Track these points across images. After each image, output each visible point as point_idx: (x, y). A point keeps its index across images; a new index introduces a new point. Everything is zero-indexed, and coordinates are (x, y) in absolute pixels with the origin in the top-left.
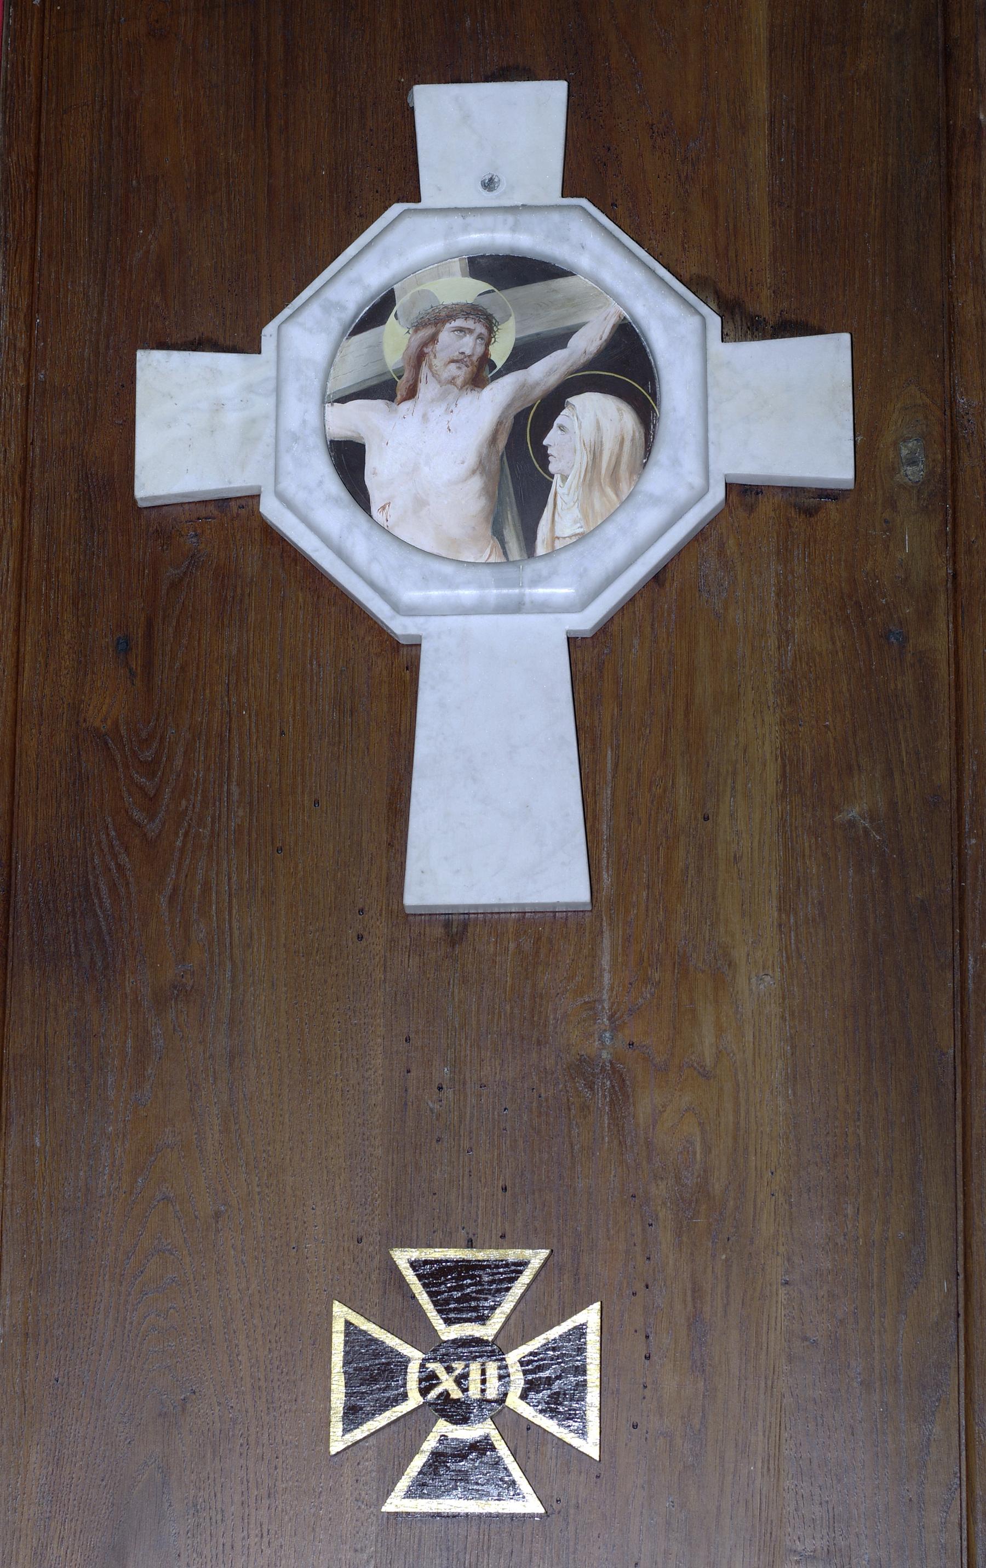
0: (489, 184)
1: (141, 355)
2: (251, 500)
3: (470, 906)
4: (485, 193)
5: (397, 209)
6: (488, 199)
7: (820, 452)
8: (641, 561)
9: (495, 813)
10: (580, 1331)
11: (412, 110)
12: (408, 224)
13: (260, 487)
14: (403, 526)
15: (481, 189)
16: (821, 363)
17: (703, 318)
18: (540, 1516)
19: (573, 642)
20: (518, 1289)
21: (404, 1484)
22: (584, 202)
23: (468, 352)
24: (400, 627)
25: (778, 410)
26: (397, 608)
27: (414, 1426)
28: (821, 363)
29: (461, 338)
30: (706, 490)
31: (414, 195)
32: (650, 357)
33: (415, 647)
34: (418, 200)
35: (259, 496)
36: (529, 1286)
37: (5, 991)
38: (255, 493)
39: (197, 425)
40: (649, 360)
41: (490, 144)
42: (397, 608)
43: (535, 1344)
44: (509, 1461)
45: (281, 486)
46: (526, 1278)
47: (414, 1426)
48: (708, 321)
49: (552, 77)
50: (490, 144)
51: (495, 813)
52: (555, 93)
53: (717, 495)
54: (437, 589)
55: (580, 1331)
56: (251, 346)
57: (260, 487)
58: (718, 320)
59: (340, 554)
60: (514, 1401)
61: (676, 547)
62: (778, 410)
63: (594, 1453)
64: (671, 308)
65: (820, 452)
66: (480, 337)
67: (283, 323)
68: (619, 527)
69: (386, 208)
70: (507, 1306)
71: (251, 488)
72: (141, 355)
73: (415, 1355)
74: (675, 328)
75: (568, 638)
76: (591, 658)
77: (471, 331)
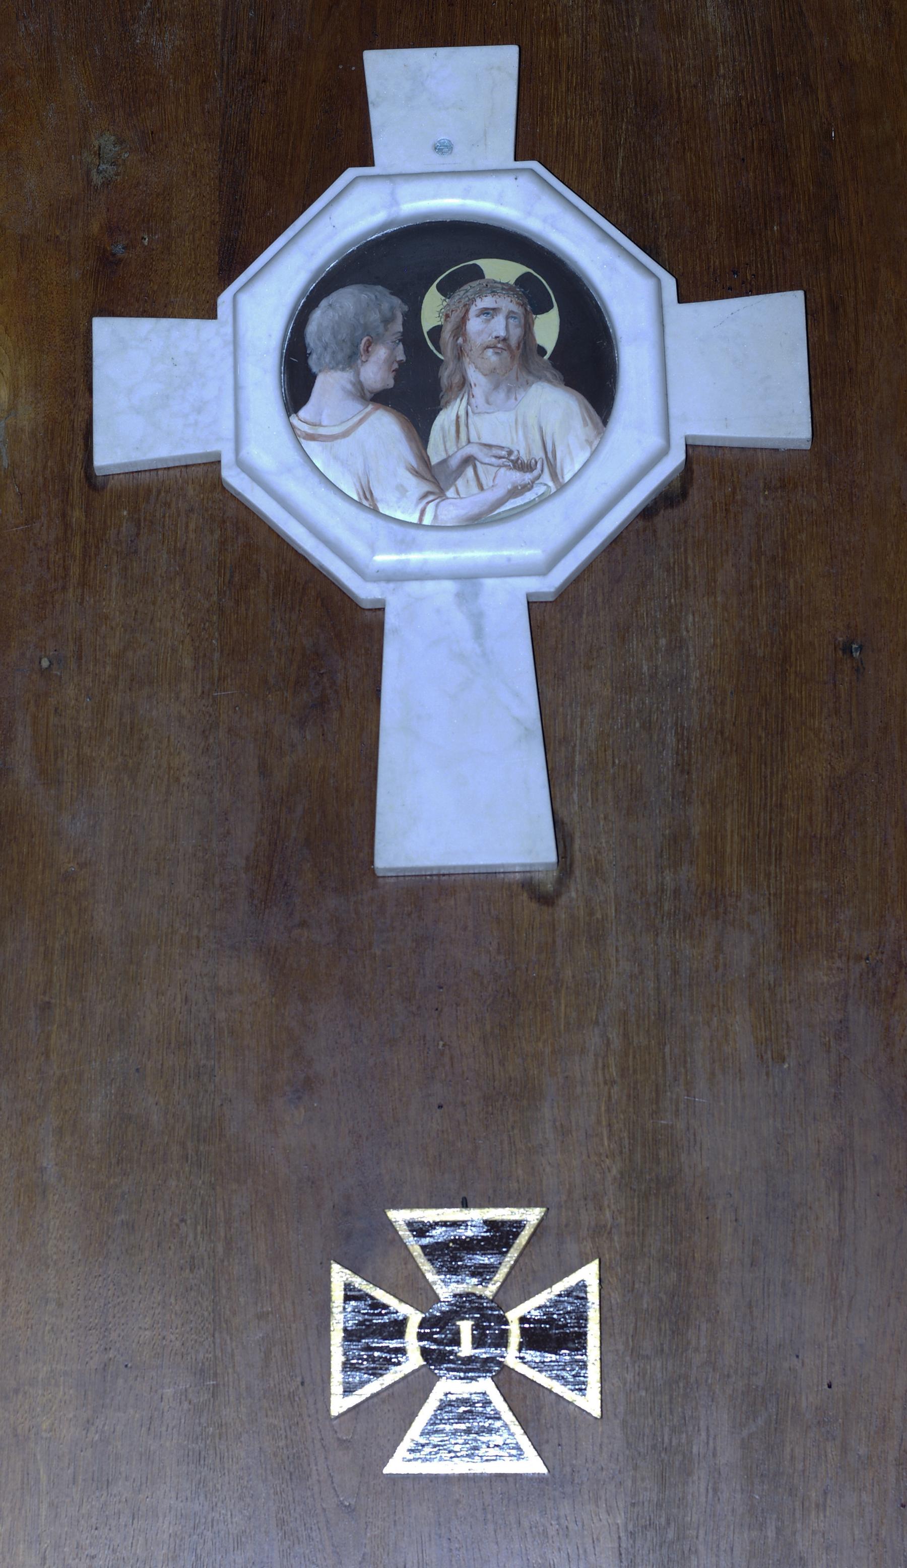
3: (426, 869)
5: (350, 173)
9: (461, 782)
10: (348, 1390)
14: (331, 488)
19: (534, 606)
21: (593, 1296)
23: (502, 334)
24: (365, 592)
25: (724, 370)
29: (488, 321)
31: (366, 159)
33: (379, 611)
39: (174, 389)
41: (443, 130)
45: (243, 453)
48: (664, 283)
50: (443, 130)
51: (461, 782)
53: (676, 459)
56: (211, 314)
57: (219, 454)
62: (724, 370)
64: (625, 268)
66: (510, 315)
71: (210, 454)
77: (495, 311)
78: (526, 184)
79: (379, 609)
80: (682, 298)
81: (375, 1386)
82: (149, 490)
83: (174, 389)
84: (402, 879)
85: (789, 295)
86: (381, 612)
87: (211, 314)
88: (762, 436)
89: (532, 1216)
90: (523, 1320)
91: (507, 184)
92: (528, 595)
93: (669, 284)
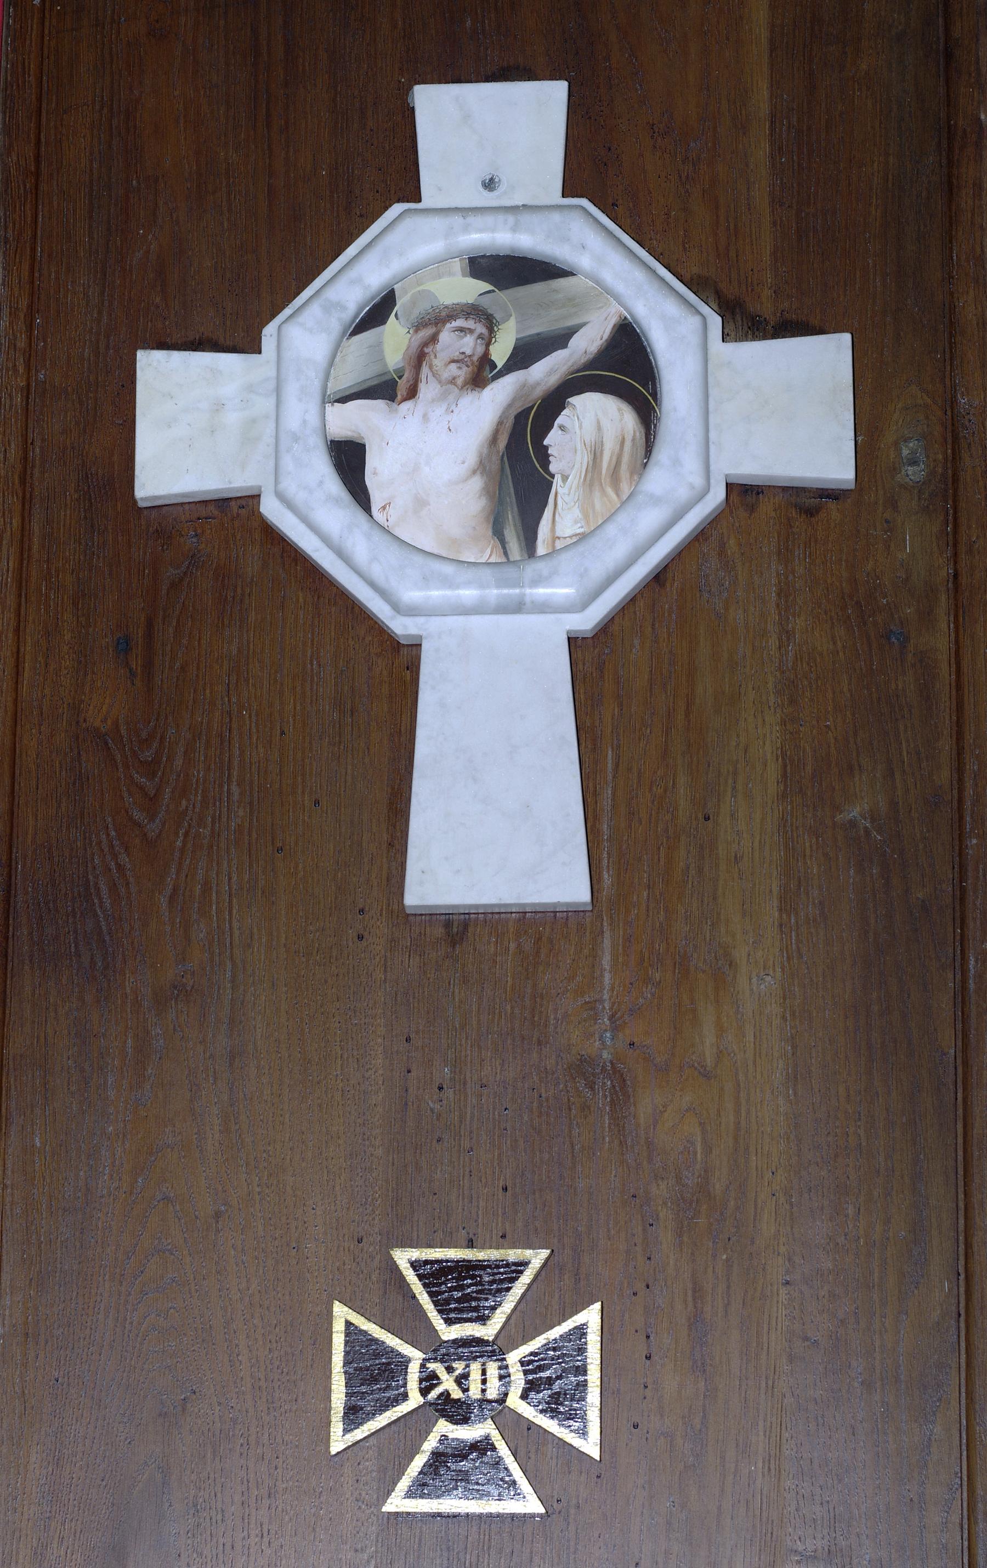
0: (490, 184)
1: (141, 355)
2: (251, 500)
3: (471, 906)
4: (485, 193)
5: (397, 209)
6: (488, 199)
7: (821, 452)
9: (496, 813)
11: (412, 110)
12: (408, 224)
13: (260, 487)
14: (403, 526)
15: (481, 189)
16: (822, 363)
17: (704, 318)
18: (541, 1516)
19: (573, 642)
20: (518, 1289)
21: (404, 1484)
22: (584, 202)
23: (468, 352)
24: (401, 627)
25: (779, 410)
26: (397, 608)
27: (415, 1426)
28: (822, 363)
29: (462, 338)
30: (706, 490)
31: (414, 195)
32: (651, 357)
33: (415, 647)
34: (419, 200)
35: (259, 496)
36: (530, 1286)
38: (255, 493)
39: (197, 425)
40: (650, 360)
42: (397, 608)
43: (536, 1344)
45: (282, 486)
46: (526, 1278)
47: (415, 1426)
48: (709, 321)
49: (553, 77)
51: (496, 813)
52: (556, 93)
53: (718, 495)
54: (438, 589)
55: (581, 1331)
56: (252, 346)
57: (260, 487)
58: (718, 320)
59: (341, 554)
60: (514, 1401)
62: (779, 410)
63: (595, 1453)
64: (671, 308)
65: (821, 452)
66: (480, 337)
67: (283, 323)
69: (386, 208)
70: (508, 1306)
71: (251, 488)
72: (141, 355)
73: (415, 1355)
74: (676, 328)
75: (569, 638)
76: (591, 658)
77: (471, 331)
81: (593, 1396)
84: (497, 916)
87: (252, 346)
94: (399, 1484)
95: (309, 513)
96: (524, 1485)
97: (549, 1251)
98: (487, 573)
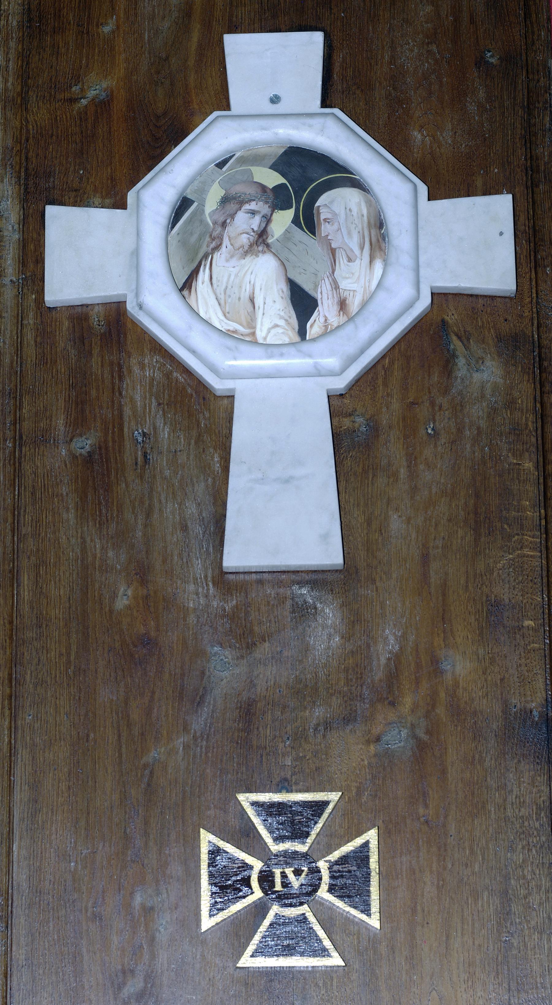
0: (275, 100)
8: (389, 331)
9: (283, 513)
16: (495, 213)
17: (415, 186)
18: (343, 966)
20: (325, 815)
21: (251, 948)
22: (337, 111)
24: (218, 385)
25: (472, 244)
27: (260, 910)
30: (417, 298)
31: (227, 107)
36: (331, 813)
37: (10, 823)
39: (92, 254)
41: (274, 77)
44: (317, 928)
45: (141, 299)
46: (331, 806)
47: (260, 910)
50: (274, 77)
51: (283, 513)
52: (317, 38)
53: (425, 302)
57: (125, 296)
58: (425, 188)
61: (396, 338)
62: (472, 244)
68: (378, 302)
69: (211, 113)
70: (320, 825)
75: (432, 293)
78: (330, 123)
79: (228, 397)
80: (431, 197)
82: (237, 586)
83: (92, 254)
85: (514, 287)
86: (230, 399)
88: (480, 286)
89: (334, 797)
90: (304, 843)
91: (317, 122)
92: (328, 391)
93: (423, 189)
94: (342, 848)
95: (160, 310)
96: (335, 954)
97: (340, 793)
98: (292, 350)
